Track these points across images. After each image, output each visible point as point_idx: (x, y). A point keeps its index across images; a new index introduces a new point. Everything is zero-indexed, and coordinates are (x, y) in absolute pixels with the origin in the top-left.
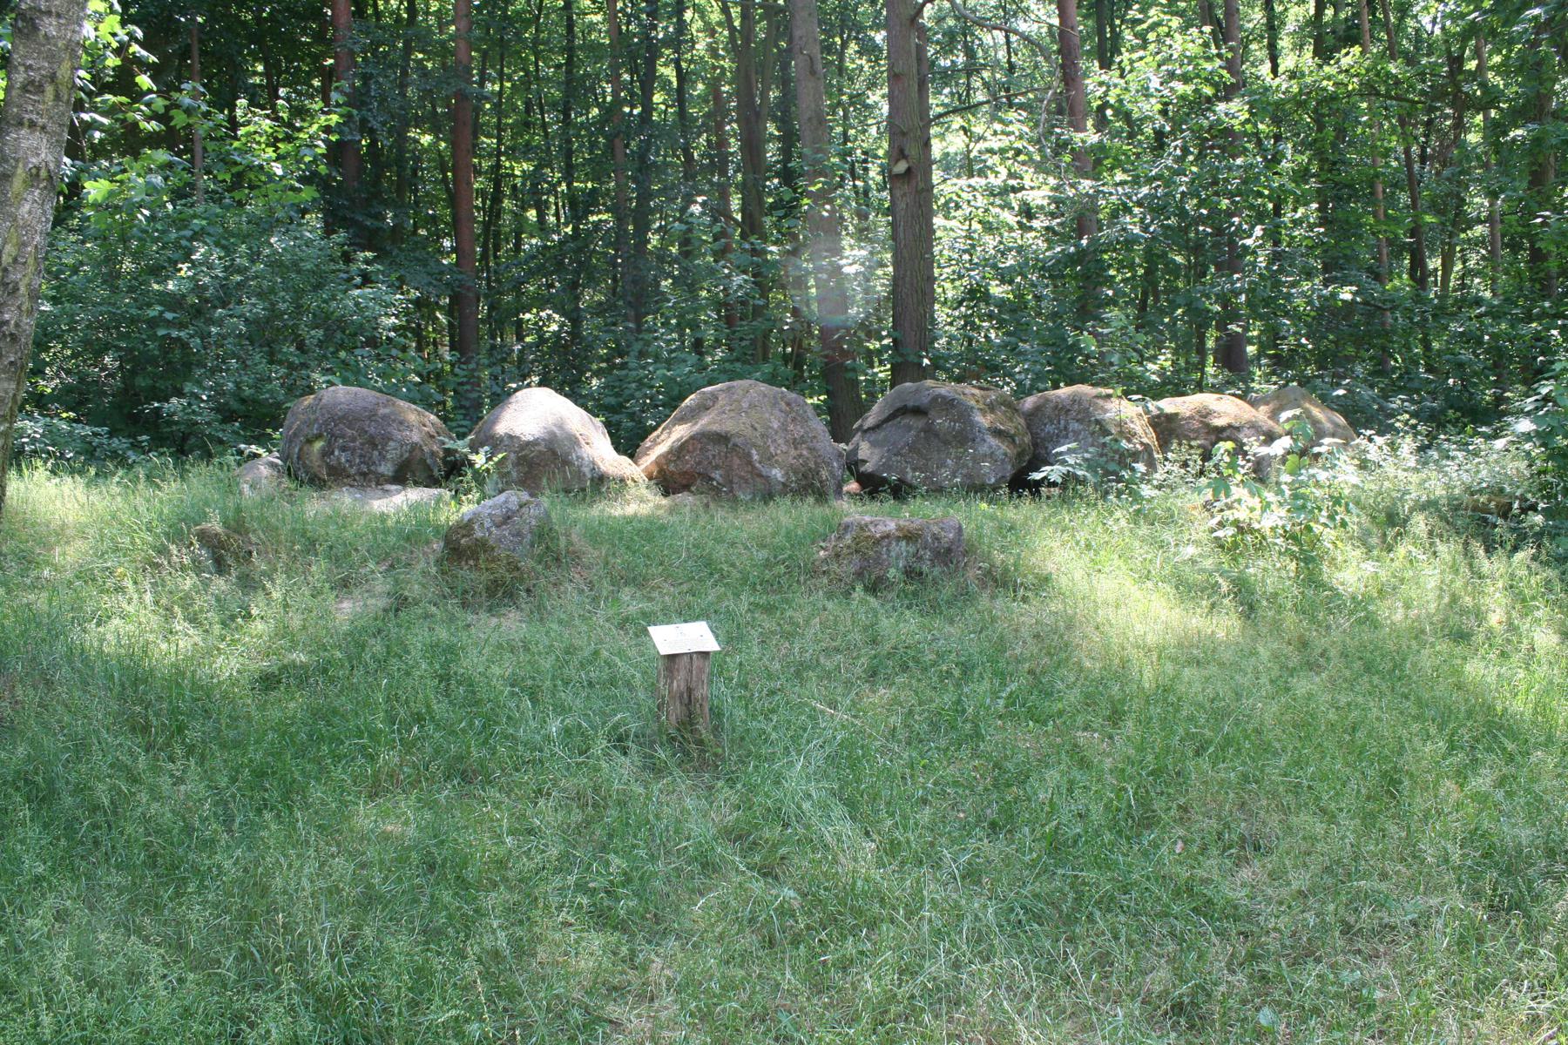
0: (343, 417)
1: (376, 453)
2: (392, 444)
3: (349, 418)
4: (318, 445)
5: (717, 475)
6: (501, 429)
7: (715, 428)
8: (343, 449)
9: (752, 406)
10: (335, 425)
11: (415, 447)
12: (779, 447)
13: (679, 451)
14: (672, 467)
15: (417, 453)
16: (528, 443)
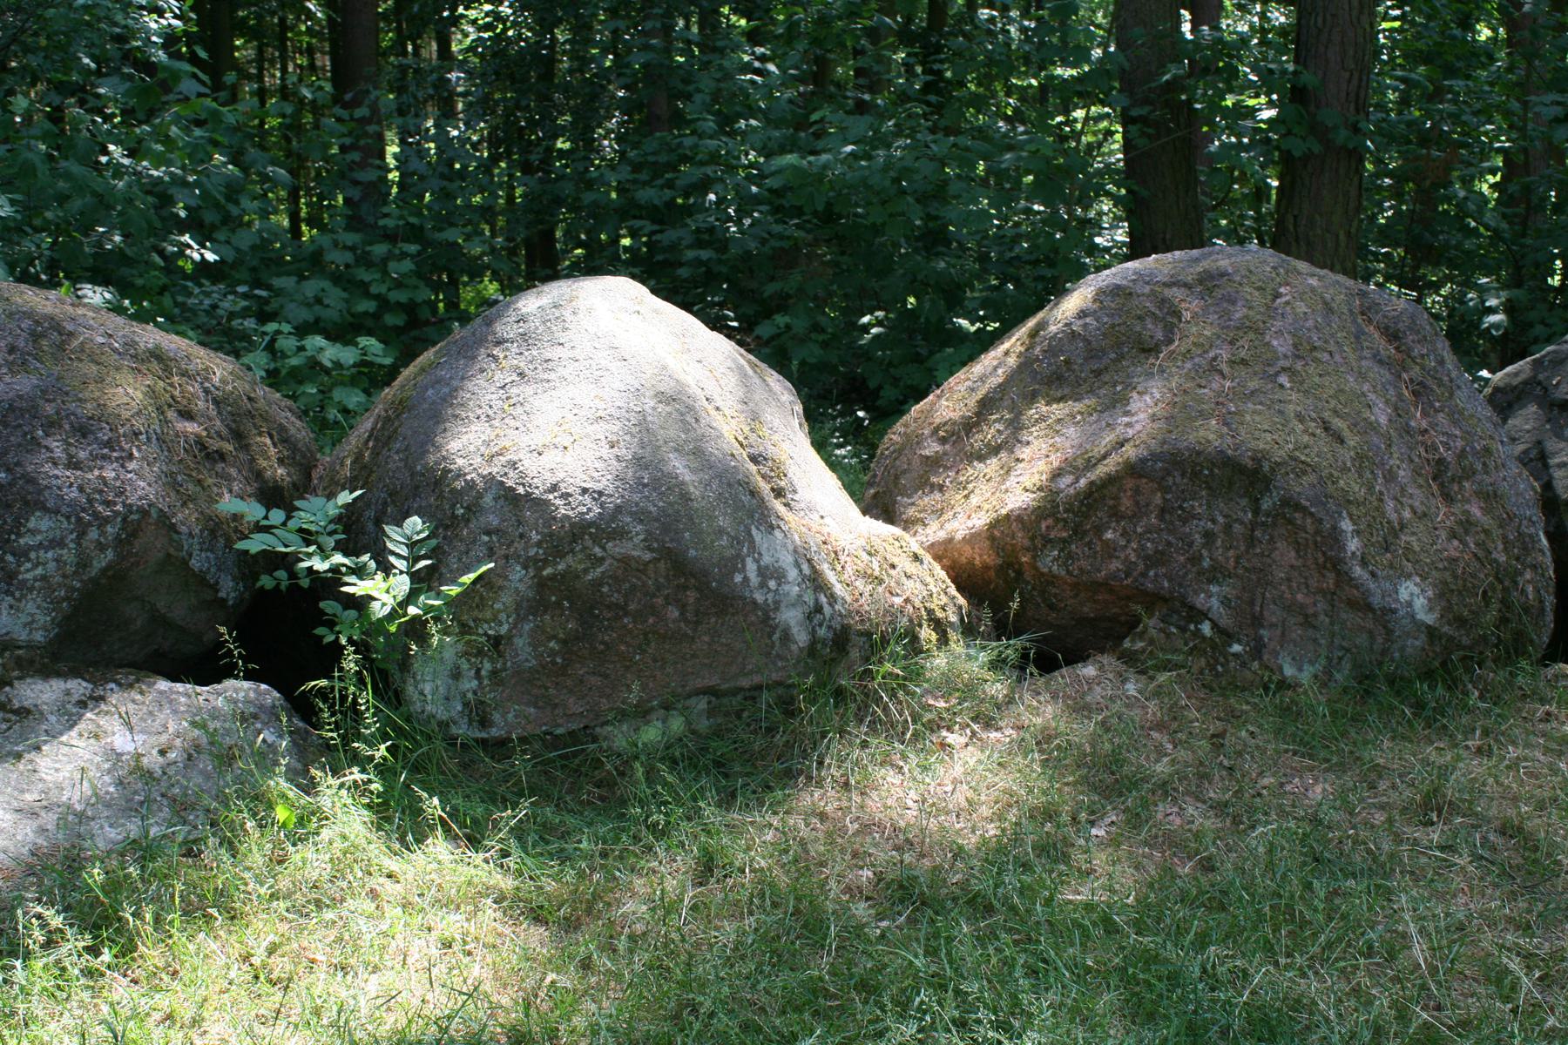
5: (1212, 599)
6: (468, 447)
7: (1209, 434)
9: (1303, 350)
11: (136, 523)
12: (1407, 499)
13: (1073, 513)
14: (1049, 562)
16: (580, 530)
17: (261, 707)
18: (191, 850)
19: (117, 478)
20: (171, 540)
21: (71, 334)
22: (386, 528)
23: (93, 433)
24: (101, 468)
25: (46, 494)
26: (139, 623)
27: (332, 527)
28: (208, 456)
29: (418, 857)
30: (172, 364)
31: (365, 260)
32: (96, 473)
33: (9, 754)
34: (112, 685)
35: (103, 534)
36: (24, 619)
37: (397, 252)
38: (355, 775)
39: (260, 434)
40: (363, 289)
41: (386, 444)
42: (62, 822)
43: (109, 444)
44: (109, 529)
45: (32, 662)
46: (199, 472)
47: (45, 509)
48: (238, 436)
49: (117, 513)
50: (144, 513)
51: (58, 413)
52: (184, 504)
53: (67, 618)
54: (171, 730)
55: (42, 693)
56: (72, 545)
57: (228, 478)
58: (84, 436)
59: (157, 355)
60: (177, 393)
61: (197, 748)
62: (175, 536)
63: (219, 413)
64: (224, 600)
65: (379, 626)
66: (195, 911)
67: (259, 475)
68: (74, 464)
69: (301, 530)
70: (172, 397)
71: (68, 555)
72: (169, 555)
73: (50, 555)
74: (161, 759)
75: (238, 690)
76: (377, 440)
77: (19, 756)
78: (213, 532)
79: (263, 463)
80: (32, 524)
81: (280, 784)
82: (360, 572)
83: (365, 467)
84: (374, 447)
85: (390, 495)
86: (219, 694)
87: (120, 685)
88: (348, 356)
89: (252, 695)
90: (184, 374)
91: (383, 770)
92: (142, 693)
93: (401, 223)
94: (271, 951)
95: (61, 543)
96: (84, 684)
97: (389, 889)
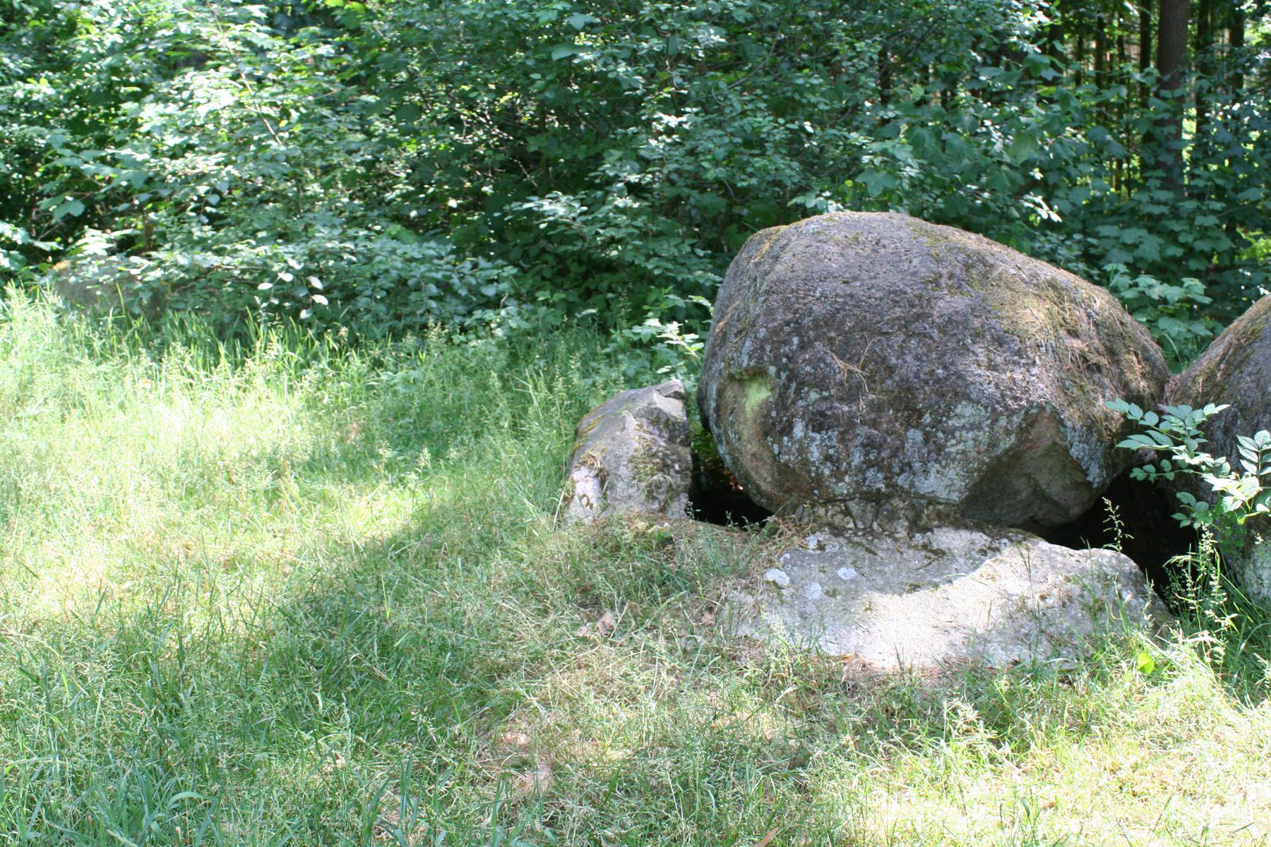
0: (830, 320)
1: (915, 435)
2: (965, 410)
3: (846, 325)
4: (757, 396)
8: (819, 422)
10: (805, 339)
11: (1034, 416)
15: (1045, 433)
17: (1122, 572)
18: (1066, 679)
19: (1024, 379)
20: (1059, 431)
21: (992, 266)
22: (1241, 439)
23: (1006, 343)
24: (1012, 371)
25: (971, 387)
26: (1024, 494)
27: (1195, 432)
28: (1088, 367)
29: (1253, 712)
30: (1064, 293)
31: (1176, 215)
32: (1009, 374)
33: (929, 583)
34: (1005, 540)
35: (1010, 422)
36: (946, 482)
37: (1204, 208)
38: (1205, 636)
39: (1129, 352)
40: (1172, 237)
41: (1239, 366)
42: (967, 642)
43: (1019, 353)
44: (1015, 419)
45: (948, 516)
46: (1082, 380)
47: (969, 399)
48: (1112, 353)
49: (1022, 407)
50: (1041, 408)
51: (982, 327)
52: (1070, 404)
53: (975, 485)
54: (1050, 581)
55: (954, 539)
56: (987, 429)
57: (1103, 386)
58: (1001, 345)
59: (1053, 285)
60: (1067, 316)
61: (1070, 598)
62: (1062, 429)
63: (1098, 334)
64: (1090, 483)
65: (1229, 520)
66: (1083, 728)
67: (1126, 385)
68: (992, 367)
69: (1171, 432)
70: (1064, 319)
71: (983, 437)
72: (1055, 443)
73: (970, 435)
74: (1041, 603)
75: (1107, 559)
76: (1229, 363)
77: (936, 586)
78: (1089, 428)
79: (1130, 376)
80: (959, 410)
81: (1141, 637)
82: (1216, 471)
83: (1216, 385)
84: (1226, 369)
85: (1241, 410)
86: (1087, 558)
87: (1011, 541)
88: (1173, 293)
89: (1114, 561)
90: (1073, 301)
91: (1232, 641)
92: (1028, 549)
93: (1210, 183)
94: (1135, 768)
95: (979, 427)
96: (985, 537)
97: (1229, 734)
